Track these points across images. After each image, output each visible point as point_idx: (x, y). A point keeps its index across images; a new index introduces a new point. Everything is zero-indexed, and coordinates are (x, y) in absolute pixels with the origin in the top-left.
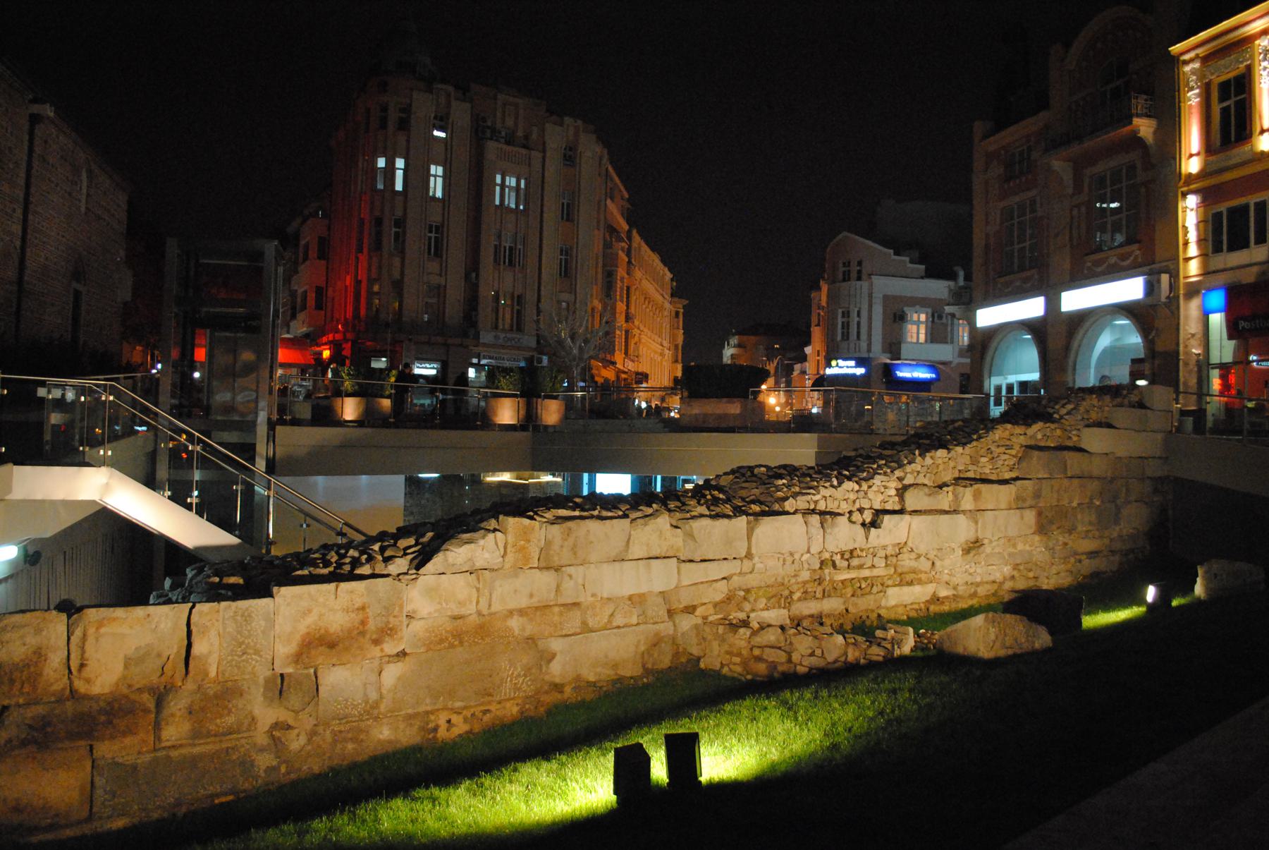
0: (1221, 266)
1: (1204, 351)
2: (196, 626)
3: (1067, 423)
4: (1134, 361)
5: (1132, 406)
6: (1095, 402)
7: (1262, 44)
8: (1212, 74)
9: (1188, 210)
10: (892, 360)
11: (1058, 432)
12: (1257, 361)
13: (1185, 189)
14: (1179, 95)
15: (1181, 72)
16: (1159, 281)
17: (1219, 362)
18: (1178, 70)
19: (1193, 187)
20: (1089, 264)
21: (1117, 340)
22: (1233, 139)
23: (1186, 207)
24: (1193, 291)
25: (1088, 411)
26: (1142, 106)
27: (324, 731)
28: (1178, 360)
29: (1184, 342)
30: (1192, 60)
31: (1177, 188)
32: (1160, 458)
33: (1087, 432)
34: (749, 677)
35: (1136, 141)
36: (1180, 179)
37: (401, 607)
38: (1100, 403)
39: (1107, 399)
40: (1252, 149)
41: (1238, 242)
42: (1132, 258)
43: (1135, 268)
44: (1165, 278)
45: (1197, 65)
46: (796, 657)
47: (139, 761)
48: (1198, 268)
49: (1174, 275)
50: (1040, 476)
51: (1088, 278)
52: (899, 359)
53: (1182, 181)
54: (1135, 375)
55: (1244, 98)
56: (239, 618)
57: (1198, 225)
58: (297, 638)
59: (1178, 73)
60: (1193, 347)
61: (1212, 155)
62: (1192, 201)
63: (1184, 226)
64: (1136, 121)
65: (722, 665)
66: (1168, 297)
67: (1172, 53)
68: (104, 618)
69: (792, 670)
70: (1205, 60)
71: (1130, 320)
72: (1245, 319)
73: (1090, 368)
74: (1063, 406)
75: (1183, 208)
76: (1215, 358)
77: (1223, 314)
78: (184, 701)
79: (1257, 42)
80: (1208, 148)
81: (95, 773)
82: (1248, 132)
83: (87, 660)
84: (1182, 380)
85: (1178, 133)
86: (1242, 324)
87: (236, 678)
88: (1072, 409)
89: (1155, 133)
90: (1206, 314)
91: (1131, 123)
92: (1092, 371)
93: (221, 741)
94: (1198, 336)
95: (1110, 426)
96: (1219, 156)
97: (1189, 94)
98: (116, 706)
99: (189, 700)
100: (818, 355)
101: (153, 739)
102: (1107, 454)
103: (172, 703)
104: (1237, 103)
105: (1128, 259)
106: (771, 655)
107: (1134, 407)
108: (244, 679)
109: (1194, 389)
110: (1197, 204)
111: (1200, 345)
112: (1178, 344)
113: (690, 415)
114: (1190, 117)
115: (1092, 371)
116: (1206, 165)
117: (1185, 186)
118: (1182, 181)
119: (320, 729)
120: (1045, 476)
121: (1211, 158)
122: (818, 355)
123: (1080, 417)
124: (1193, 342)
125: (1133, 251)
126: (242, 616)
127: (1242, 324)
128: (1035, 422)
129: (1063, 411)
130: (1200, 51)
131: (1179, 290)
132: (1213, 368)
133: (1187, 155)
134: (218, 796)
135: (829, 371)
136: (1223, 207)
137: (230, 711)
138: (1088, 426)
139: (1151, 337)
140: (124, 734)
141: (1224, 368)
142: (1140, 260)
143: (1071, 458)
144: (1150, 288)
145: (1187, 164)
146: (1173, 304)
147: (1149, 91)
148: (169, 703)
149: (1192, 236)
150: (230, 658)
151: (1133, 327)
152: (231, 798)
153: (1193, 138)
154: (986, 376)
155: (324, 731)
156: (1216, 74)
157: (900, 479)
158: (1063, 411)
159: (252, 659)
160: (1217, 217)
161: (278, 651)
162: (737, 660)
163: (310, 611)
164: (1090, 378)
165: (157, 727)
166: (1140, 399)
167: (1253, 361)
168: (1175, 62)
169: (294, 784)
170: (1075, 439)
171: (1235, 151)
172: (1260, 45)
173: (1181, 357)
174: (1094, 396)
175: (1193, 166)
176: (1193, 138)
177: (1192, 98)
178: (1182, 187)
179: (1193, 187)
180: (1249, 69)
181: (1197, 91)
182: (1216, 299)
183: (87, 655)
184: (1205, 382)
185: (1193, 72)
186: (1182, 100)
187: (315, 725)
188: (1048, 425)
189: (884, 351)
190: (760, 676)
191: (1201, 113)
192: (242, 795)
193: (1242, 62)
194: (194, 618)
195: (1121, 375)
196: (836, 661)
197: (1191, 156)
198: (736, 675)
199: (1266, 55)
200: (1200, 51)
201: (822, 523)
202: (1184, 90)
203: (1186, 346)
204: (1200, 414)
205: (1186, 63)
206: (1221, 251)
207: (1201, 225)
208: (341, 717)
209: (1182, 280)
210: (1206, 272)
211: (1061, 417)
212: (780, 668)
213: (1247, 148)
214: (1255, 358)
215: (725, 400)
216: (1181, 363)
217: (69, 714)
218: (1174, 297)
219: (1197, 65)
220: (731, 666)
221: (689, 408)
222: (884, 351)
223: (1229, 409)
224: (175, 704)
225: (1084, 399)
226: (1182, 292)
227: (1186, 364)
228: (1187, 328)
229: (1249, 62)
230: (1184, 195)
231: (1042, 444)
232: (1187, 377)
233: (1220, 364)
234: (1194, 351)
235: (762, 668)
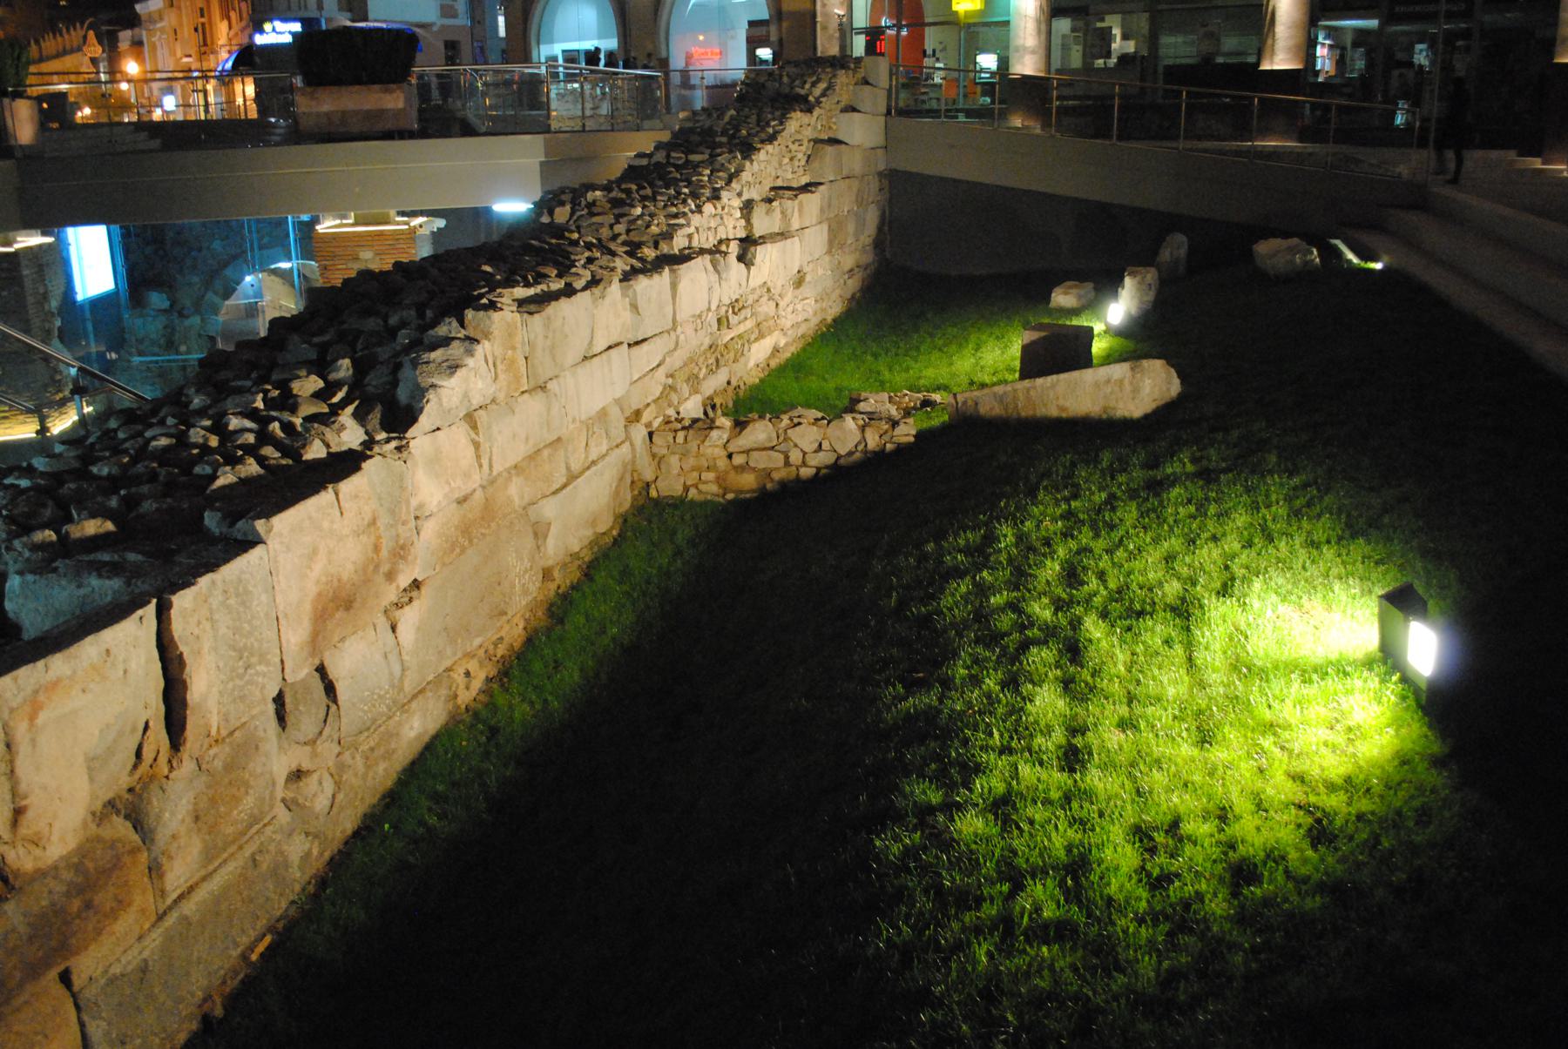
2: (187, 644)
10: (353, 21)
27: (353, 758)
28: (815, 23)
34: (730, 496)
37: (408, 502)
46: (795, 457)
47: (146, 954)
52: (366, 19)
56: (232, 601)
58: (307, 607)
65: (686, 489)
68: (36, 692)
69: (793, 475)
78: (184, 801)
81: (85, 1018)
83: (26, 797)
87: (243, 720)
93: (241, 848)
98: (90, 865)
99: (191, 795)
100: (202, 16)
101: (152, 900)
103: (167, 815)
106: (761, 461)
108: (253, 717)
113: (318, 115)
119: (347, 756)
122: (202, 16)
126: (237, 595)
132: (857, 33)
134: (251, 949)
135: (260, 40)
137: (247, 785)
140: (113, 915)
148: (159, 817)
150: (230, 685)
152: (268, 939)
154: (533, 43)
155: (353, 758)
157: (740, 195)
159: (258, 674)
161: (288, 641)
162: (710, 476)
163: (315, 551)
165: (155, 870)
169: (339, 863)
173: (819, 19)
183: (23, 787)
187: (339, 754)
189: (340, 9)
190: (748, 492)
192: (280, 926)
194: (178, 627)
196: (850, 453)
198: (709, 497)
201: (715, 267)
208: (368, 724)
212: (776, 476)
215: (376, 87)
216: (818, 26)
217: (22, 929)
220: (702, 487)
221: (314, 103)
222: (340, 9)
224: (173, 814)
227: (825, 28)
234: (836, 11)
235: (748, 481)
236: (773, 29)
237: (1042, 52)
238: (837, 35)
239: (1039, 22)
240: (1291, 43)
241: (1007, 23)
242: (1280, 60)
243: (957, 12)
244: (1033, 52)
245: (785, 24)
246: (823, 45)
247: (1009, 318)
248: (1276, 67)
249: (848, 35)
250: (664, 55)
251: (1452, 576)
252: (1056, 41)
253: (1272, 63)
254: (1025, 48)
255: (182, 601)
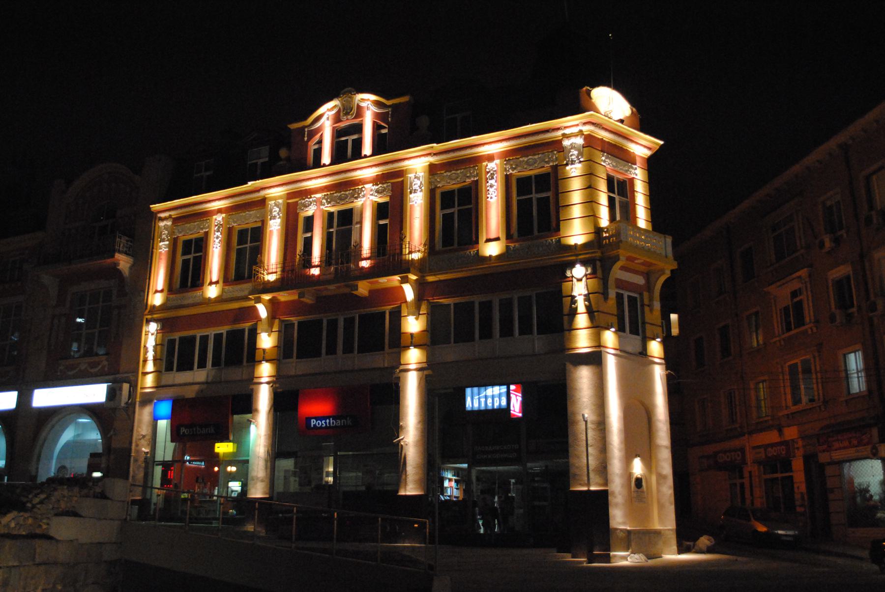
0: (170, 383)
1: (151, 451)
3: (39, 512)
4: (93, 455)
5: (95, 496)
6: (66, 492)
7: (218, 219)
8: (180, 232)
9: (150, 334)
11: (30, 521)
12: (190, 461)
13: (149, 317)
14: (153, 241)
15: (157, 226)
16: (121, 389)
17: (162, 460)
18: (155, 224)
19: (155, 316)
20: (61, 368)
21: (78, 435)
22: (189, 284)
23: (149, 332)
24: (147, 400)
25: (59, 501)
26: (124, 245)
28: (130, 456)
29: (136, 442)
30: (165, 219)
31: (143, 315)
32: (115, 543)
33: (56, 520)
35: (114, 271)
36: (146, 309)
38: (70, 494)
39: (76, 489)
40: (202, 294)
41: (185, 365)
42: (100, 366)
43: (101, 375)
44: (126, 387)
45: (169, 223)
48: (153, 382)
49: (134, 385)
50: (11, 564)
51: (60, 380)
53: (147, 311)
54: (92, 468)
55: (201, 256)
57: (155, 347)
59: (155, 227)
60: (143, 446)
61: (173, 294)
62: (153, 327)
63: (145, 346)
64: (118, 256)
66: (127, 403)
67: (152, 210)
70: (176, 220)
71: (93, 419)
72: (186, 427)
73: (52, 458)
74: (36, 496)
75: (146, 332)
76: (159, 457)
77: (170, 420)
79: (214, 217)
80: (171, 288)
82: (201, 281)
84: (131, 473)
85: (149, 269)
86: (183, 430)
88: (45, 499)
89: (131, 268)
90: (155, 419)
91: (113, 256)
92: (54, 461)
94: (148, 437)
95: (75, 514)
96: (178, 295)
97: (161, 244)
102: (71, 541)
104: (194, 257)
105: (96, 367)
107: (97, 497)
109: (141, 483)
110: (157, 330)
111: (148, 445)
112: (131, 443)
114: (159, 262)
115: (54, 461)
116: (167, 300)
117: (150, 315)
118: (147, 311)
120: (16, 564)
121: (171, 296)
123: (51, 506)
124: (143, 442)
125: (102, 361)
127: (183, 430)
128: (9, 512)
129: (36, 500)
130: (173, 213)
131: (136, 398)
132: (157, 465)
133: (154, 290)
136: (176, 336)
138: (56, 515)
139: (109, 436)
141: (166, 465)
142: (106, 369)
143: (40, 545)
144: (112, 394)
145: (153, 298)
146: (130, 410)
147: (130, 234)
149: (150, 355)
151: (94, 425)
153: (159, 278)
156: (183, 234)
158: (36, 500)
160: (171, 342)
164: (49, 469)
166: (102, 491)
167: (187, 461)
168: (153, 217)
170: (45, 527)
171: (190, 294)
172: (216, 219)
173: (133, 454)
174: (65, 487)
175: (157, 300)
176: (159, 278)
177: (162, 248)
178: (146, 315)
179: (155, 316)
180: (207, 234)
181: (167, 243)
182: (165, 408)
184: (150, 477)
185: (166, 227)
186: (155, 247)
188: (22, 514)
191: (168, 258)
193: (202, 229)
195: (80, 465)
197: (157, 291)
199: (219, 228)
200: (173, 213)
202: (157, 240)
203: (137, 445)
204: (144, 504)
205: (162, 219)
206: (172, 370)
207: (159, 347)
209: (139, 390)
210: (159, 385)
211: (34, 506)
213: (198, 293)
214: (188, 458)
216: (132, 459)
218: (131, 403)
219: (169, 223)
223: (167, 499)
225: (55, 490)
226: (138, 400)
227: (136, 461)
228: (140, 430)
229: (207, 230)
230: (148, 322)
231: (15, 532)
232: (136, 471)
233: (164, 461)
234: (143, 449)
236: (104, 460)
237: (267, 480)
238: (143, 465)
239: (266, 461)
240: (417, 477)
241: (247, 462)
242: (410, 489)
243: (218, 454)
244: (262, 481)
245: (112, 457)
246: (134, 471)
247: (598, 407)
248: (408, 493)
249: (150, 465)
250: (33, 473)
251: (834, 454)
252: (280, 475)
253: (405, 490)
254: (258, 478)
255: (616, 317)
